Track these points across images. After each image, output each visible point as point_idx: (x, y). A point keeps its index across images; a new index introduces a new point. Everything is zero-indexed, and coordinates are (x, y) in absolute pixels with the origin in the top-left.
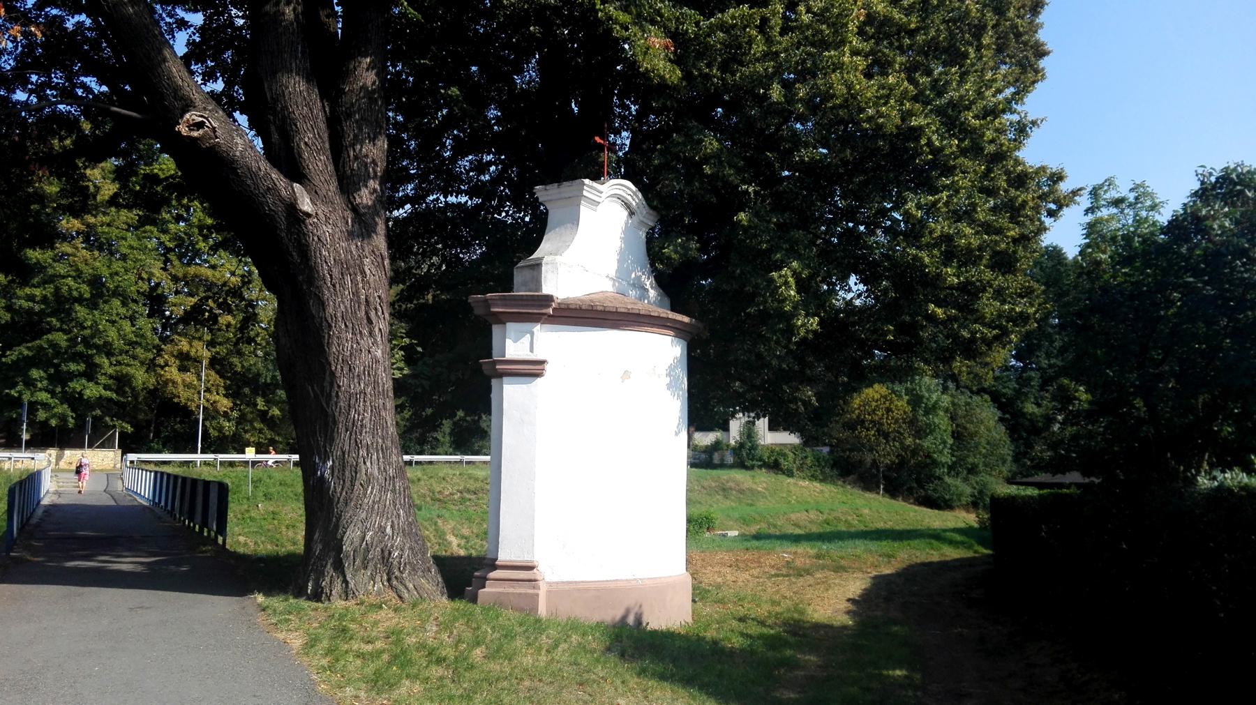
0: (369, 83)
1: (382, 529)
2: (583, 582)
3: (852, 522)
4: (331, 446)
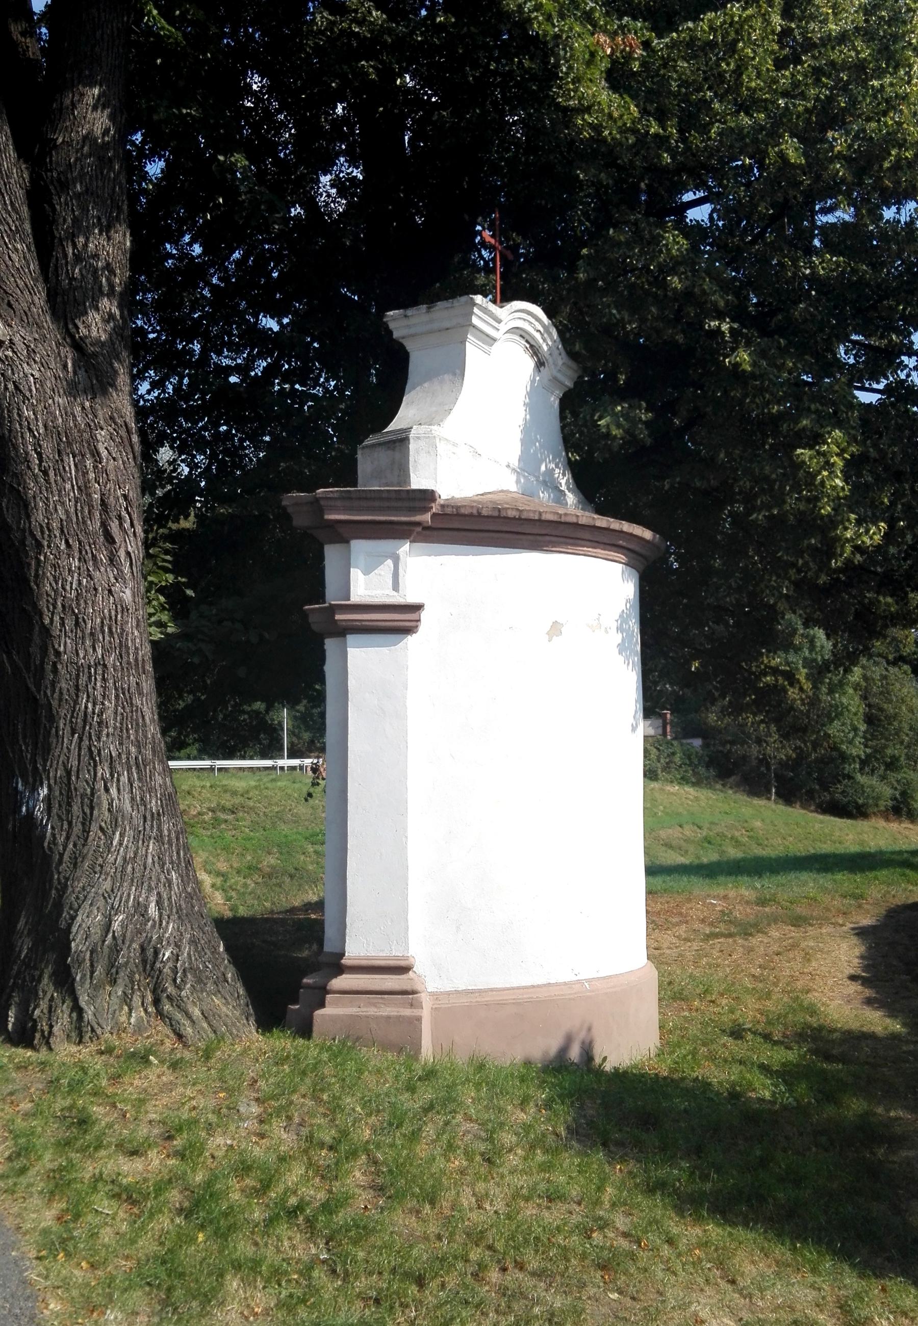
0: (98, 132)
1: (141, 909)
2: (492, 990)
3: (740, 839)
4: (45, 761)
